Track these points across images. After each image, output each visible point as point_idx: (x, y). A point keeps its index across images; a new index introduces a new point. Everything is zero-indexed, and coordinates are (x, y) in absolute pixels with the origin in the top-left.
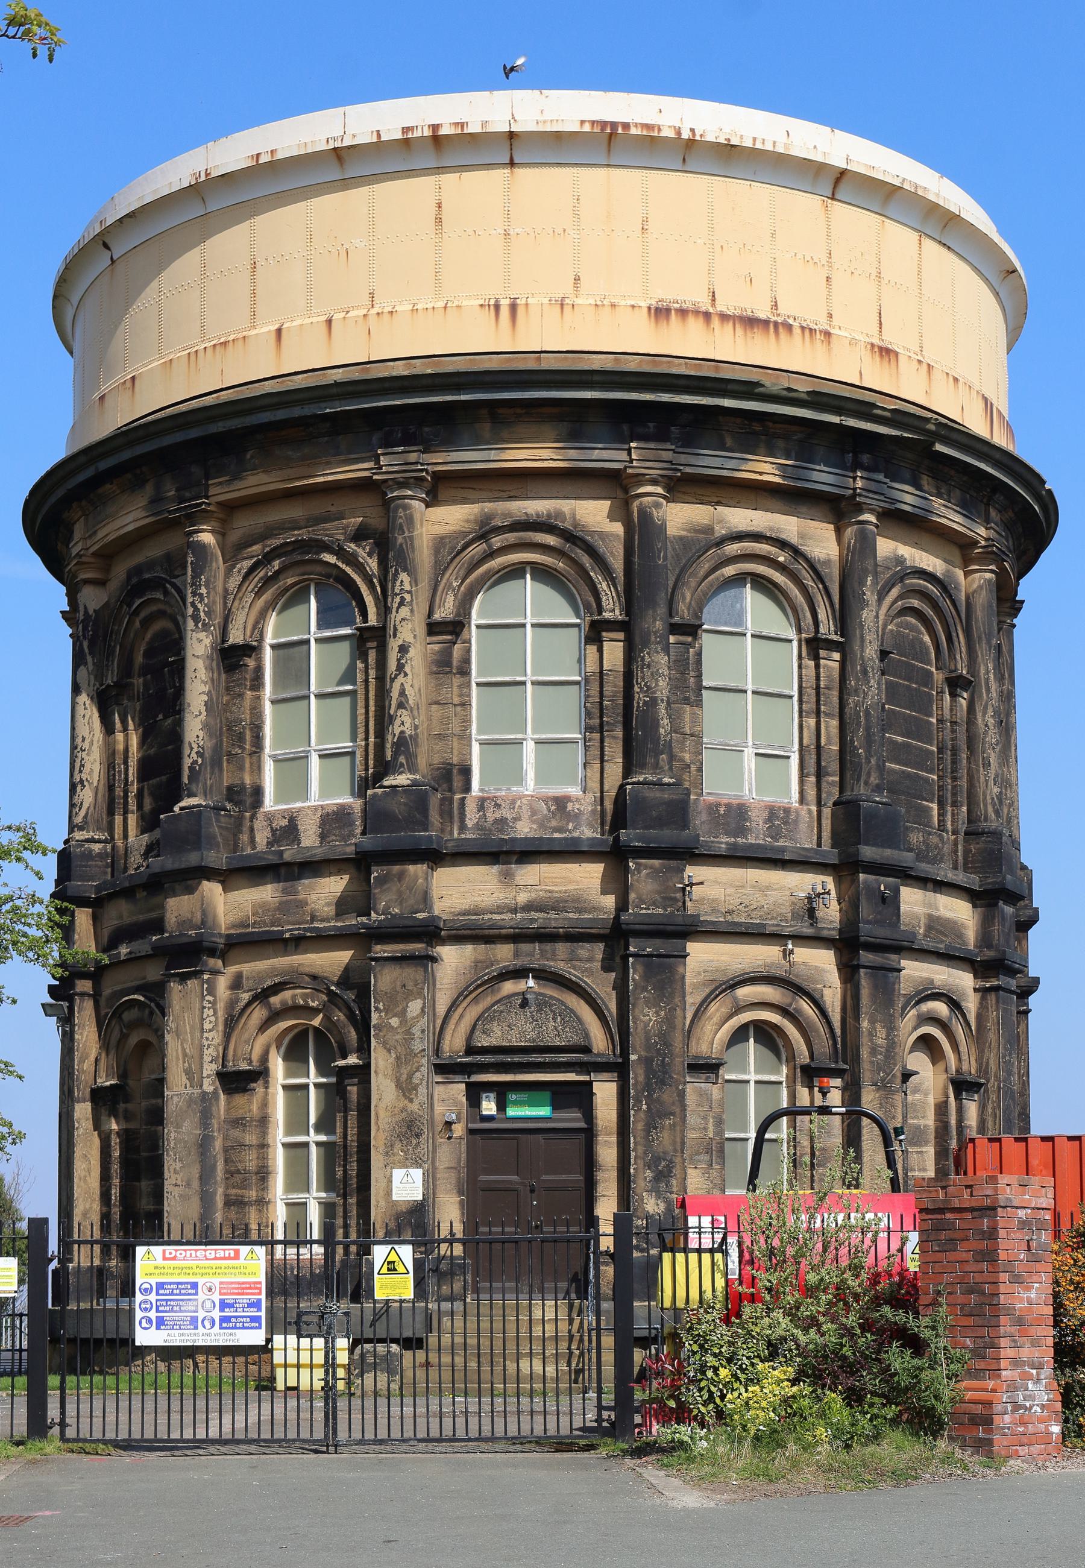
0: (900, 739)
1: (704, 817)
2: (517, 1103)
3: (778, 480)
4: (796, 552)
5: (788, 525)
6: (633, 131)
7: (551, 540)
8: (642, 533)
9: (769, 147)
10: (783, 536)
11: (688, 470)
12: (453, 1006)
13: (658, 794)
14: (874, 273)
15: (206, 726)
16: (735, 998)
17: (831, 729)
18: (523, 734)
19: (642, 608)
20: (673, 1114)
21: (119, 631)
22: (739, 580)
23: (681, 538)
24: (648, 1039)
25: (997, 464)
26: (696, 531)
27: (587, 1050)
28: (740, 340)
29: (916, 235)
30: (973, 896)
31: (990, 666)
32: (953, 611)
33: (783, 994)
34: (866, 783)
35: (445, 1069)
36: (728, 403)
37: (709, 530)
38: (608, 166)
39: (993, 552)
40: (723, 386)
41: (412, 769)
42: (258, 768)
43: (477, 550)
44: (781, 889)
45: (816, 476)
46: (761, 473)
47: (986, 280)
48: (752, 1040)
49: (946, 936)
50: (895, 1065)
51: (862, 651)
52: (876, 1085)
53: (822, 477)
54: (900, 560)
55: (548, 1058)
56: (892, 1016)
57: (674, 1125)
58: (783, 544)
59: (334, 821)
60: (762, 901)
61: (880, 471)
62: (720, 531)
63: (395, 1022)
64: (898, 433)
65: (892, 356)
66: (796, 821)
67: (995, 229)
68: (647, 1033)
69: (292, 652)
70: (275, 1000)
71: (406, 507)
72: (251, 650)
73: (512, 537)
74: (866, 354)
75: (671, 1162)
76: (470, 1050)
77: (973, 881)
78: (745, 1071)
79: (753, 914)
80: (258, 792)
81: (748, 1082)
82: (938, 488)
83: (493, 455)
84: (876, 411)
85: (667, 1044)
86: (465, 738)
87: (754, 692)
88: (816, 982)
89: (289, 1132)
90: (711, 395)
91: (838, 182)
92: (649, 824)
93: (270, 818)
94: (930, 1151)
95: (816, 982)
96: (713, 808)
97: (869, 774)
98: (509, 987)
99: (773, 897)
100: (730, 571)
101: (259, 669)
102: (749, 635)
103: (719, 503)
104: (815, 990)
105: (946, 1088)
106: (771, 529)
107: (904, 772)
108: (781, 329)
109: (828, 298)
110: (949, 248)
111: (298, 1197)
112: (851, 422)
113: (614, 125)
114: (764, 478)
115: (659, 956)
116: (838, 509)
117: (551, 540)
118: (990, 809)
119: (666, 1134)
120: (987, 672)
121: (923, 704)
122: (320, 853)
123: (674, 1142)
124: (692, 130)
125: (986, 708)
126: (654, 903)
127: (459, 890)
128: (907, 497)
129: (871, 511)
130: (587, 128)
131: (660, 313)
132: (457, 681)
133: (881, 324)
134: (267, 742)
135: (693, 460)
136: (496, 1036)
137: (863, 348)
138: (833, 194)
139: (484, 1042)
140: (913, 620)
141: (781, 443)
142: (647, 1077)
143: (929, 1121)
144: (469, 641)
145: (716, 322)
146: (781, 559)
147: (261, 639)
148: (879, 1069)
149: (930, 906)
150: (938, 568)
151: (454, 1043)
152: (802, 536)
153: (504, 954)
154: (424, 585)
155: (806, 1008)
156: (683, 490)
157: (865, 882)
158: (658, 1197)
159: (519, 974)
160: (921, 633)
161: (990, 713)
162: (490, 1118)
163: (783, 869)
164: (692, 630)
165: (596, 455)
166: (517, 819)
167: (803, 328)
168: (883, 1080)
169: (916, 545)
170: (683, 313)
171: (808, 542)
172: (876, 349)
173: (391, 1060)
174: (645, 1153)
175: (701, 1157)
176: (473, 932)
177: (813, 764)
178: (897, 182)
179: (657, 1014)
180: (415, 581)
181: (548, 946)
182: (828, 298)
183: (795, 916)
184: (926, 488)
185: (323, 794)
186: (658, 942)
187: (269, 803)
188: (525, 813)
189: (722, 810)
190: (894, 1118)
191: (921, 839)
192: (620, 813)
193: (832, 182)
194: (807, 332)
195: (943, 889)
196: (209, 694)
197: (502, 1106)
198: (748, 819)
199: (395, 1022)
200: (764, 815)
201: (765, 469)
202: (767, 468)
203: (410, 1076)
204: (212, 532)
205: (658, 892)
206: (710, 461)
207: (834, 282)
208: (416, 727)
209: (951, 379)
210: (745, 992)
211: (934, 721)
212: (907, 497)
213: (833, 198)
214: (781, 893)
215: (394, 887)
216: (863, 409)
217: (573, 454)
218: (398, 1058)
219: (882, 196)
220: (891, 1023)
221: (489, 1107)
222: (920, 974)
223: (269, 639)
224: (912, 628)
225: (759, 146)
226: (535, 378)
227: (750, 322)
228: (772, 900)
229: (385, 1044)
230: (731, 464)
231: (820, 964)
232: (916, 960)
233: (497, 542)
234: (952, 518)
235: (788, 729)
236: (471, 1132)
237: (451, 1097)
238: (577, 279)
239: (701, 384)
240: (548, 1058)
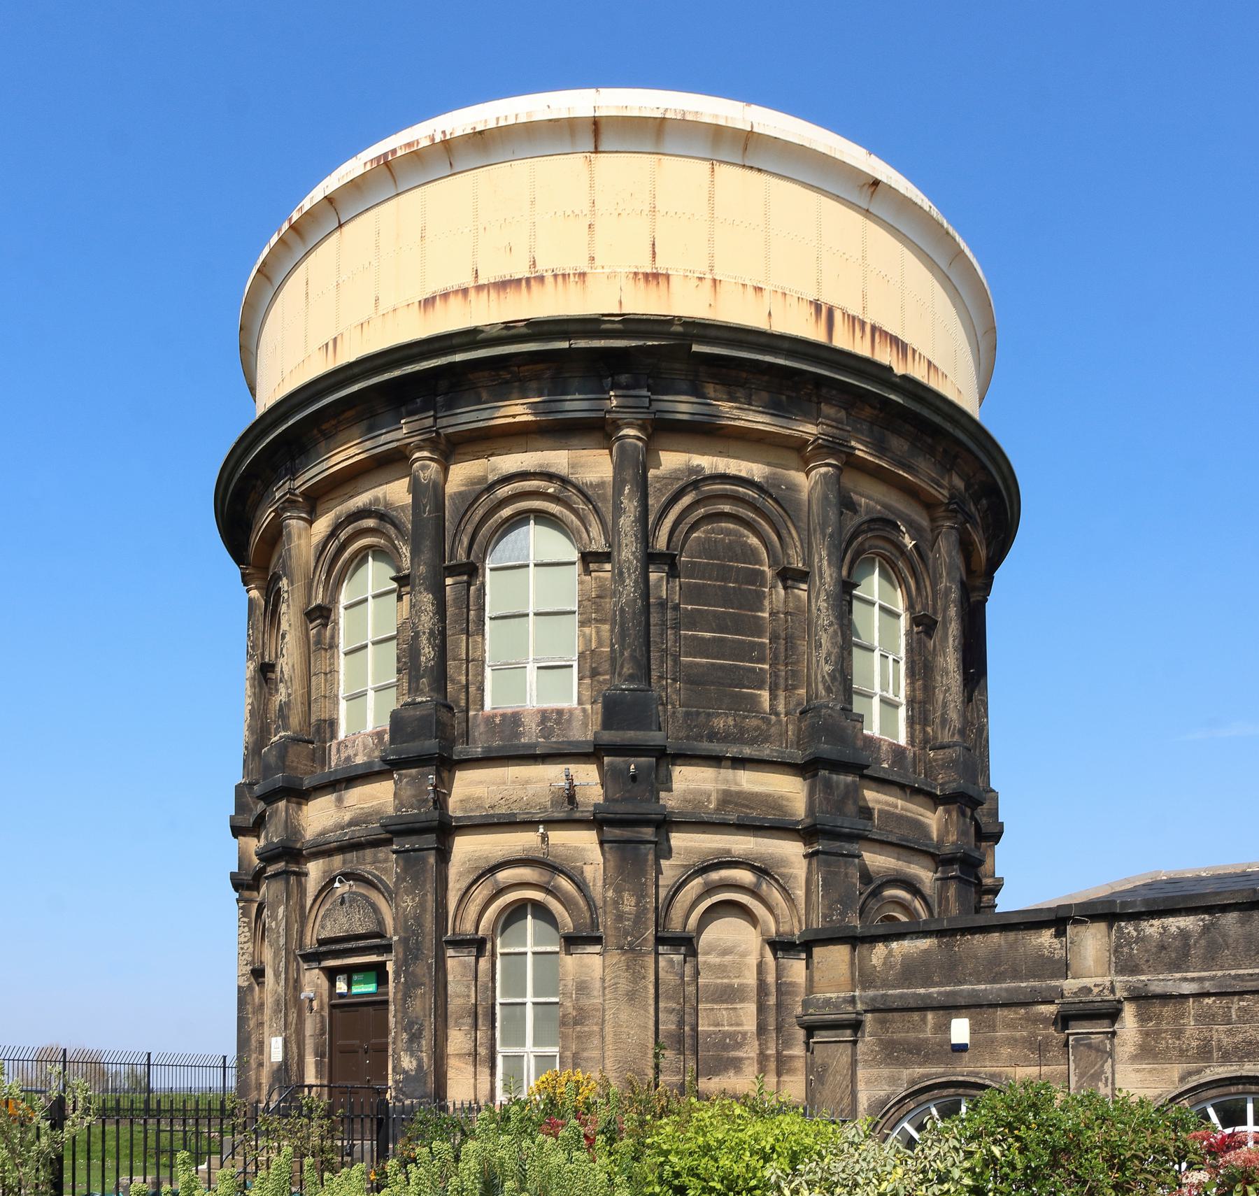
0: (708, 635)
1: (482, 728)
2: (359, 982)
3: (531, 418)
4: (564, 481)
5: (558, 459)
6: (399, 153)
8: (429, 496)
9: (511, 121)
10: (552, 470)
11: (450, 430)
13: (412, 713)
14: (647, 208)
16: (496, 881)
17: (603, 633)
19: (446, 565)
20: (423, 984)
22: (520, 519)
23: (460, 493)
24: (406, 921)
25: (790, 354)
26: (473, 484)
28: (493, 304)
29: (707, 165)
30: (805, 769)
31: (824, 553)
32: (779, 509)
33: (541, 874)
34: (620, 675)
35: (308, 958)
36: (458, 357)
38: (398, 195)
39: (821, 446)
40: (448, 343)
41: (286, 728)
44: (540, 781)
45: (568, 406)
46: (514, 416)
47: (837, 198)
48: (529, 917)
49: (752, 808)
50: (647, 929)
51: (619, 554)
52: (622, 948)
53: (576, 405)
54: (699, 469)
55: (353, 945)
56: (645, 884)
57: (424, 994)
58: (549, 476)
60: (521, 794)
61: (640, 387)
62: (492, 478)
64: (640, 343)
65: (662, 281)
66: (569, 721)
67: (863, 151)
68: (405, 916)
71: (288, 526)
74: (629, 285)
75: (421, 1025)
77: (799, 756)
78: (525, 945)
79: (513, 806)
81: (526, 954)
82: (729, 393)
83: (325, 465)
84: (604, 326)
85: (420, 925)
86: (335, 699)
87: (536, 614)
88: (576, 860)
90: (445, 355)
91: (597, 133)
94: (751, 1008)
95: (576, 860)
96: (489, 720)
97: (622, 667)
99: (531, 789)
100: (506, 512)
102: (532, 566)
103: (492, 455)
104: (573, 868)
105: (762, 949)
106: (541, 466)
107: (713, 664)
108: (533, 282)
109: (591, 243)
110: (760, 170)
112: (582, 344)
113: (385, 155)
114: (518, 419)
115: (415, 850)
116: (596, 430)
118: (821, 687)
119: (418, 1002)
120: (821, 560)
121: (756, 601)
123: (424, 1008)
124: (444, 132)
125: (818, 593)
126: (412, 807)
128: (683, 407)
129: (630, 425)
130: (368, 167)
131: (428, 303)
133: (654, 253)
135: (453, 420)
137: (624, 279)
138: (596, 147)
140: (731, 526)
141: (534, 385)
142: (405, 954)
143: (751, 979)
144: (337, 624)
145: (472, 294)
146: (551, 490)
148: (626, 934)
149: (726, 781)
150: (755, 472)
152: (573, 466)
153: (337, 861)
154: (300, 584)
155: (565, 884)
156: (462, 451)
157: (611, 764)
158: (411, 1056)
160: (742, 536)
161: (823, 596)
162: (341, 996)
163: (543, 763)
164: (472, 571)
165: (383, 439)
166: (356, 755)
167: (556, 276)
168: (630, 944)
169: (721, 454)
170: (445, 296)
171: (579, 470)
172: (640, 276)
174: (403, 1019)
175: (465, 1020)
177: (590, 667)
178: (658, 114)
179: (413, 900)
180: (291, 583)
181: (361, 853)
182: (591, 243)
183: (555, 803)
184: (712, 394)
186: (414, 838)
189: (497, 720)
190: (644, 978)
191: (732, 723)
193: (592, 135)
194: (560, 279)
195: (747, 765)
196: (252, 704)
197: (349, 986)
198: (522, 724)
200: (538, 719)
201: (517, 411)
202: (519, 410)
204: (256, 588)
205: (414, 796)
206: (468, 418)
207: (597, 227)
208: (289, 695)
209: (750, 291)
210: (504, 876)
211: (766, 615)
212: (683, 407)
213: (596, 151)
214: (541, 785)
216: (589, 327)
217: (368, 444)
219: (653, 133)
220: (642, 891)
221: (341, 987)
222: (708, 845)
224: (729, 532)
225: (502, 123)
226: (320, 386)
227: (503, 285)
228: (530, 793)
230: (485, 415)
231: (582, 845)
232: (704, 832)
234: (757, 420)
235: (568, 641)
236: (332, 1007)
237: (313, 981)
238: (377, 300)
239: (431, 347)
240: (353, 945)
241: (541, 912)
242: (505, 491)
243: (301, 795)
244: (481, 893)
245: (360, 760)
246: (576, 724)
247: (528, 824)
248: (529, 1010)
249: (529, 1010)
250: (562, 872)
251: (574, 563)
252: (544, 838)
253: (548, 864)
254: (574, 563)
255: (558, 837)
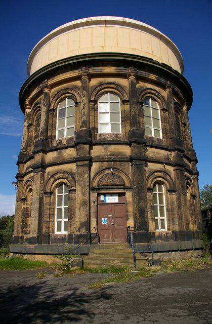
7: (114, 86)
12: (95, 176)
15: (44, 124)
18: (108, 118)
21: (110, 241)
27: (124, 185)
37: (143, 87)
42: (55, 132)
43: (99, 88)
53: (163, 81)
55: (116, 187)
58: (157, 91)
59: (69, 140)
63: (81, 179)
69: (62, 112)
70: (56, 177)
72: (54, 110)
73: (106, 86)
76: (98, 186)
80: (55, 136)
89: (58, 206)
92: (137, 138)
93: (56, 141)
98: (107, 172)
101: (56, 114)
111: (59, 220)
117: (114, 86)
122: (66, 146)
127: (97, 151)
132: (95, 112)
134: (57, 127)
136: (104, 182)
139: (102, 184)
147: (57, 108)
151: (95, 184)
153: (105, 164)
159: (109, 168)
173: (81, 187)
176: (99, 159)
185: (67, 135)
187: (57, 138)
188: (109, 137)
192: (132, 134)
199: (81, 179)
201: (153, 77)
203: (85, 191)
215: (81, 151)
218: (82, 187)
223: (58, 109)
229: (79, 184)
233: (103, 87)
240: (116, 187)
241: (65, 184)
242: (148, 91)
243: (45, 152)
244: (52, 180)
245: (109, 139)
246: (164, 143)
247: (162, 163)
248: (158, 207)
249: (158, 207)
250: (169, 175)
251: (107, 124)
252: (164, 166)
253: (165, 172)
254: (107, 124)
255: (167, 167)
